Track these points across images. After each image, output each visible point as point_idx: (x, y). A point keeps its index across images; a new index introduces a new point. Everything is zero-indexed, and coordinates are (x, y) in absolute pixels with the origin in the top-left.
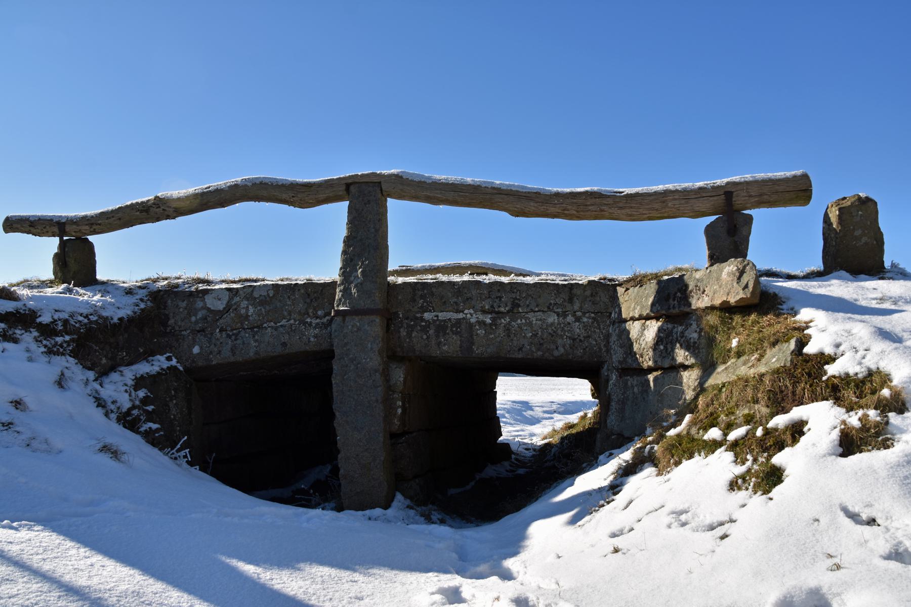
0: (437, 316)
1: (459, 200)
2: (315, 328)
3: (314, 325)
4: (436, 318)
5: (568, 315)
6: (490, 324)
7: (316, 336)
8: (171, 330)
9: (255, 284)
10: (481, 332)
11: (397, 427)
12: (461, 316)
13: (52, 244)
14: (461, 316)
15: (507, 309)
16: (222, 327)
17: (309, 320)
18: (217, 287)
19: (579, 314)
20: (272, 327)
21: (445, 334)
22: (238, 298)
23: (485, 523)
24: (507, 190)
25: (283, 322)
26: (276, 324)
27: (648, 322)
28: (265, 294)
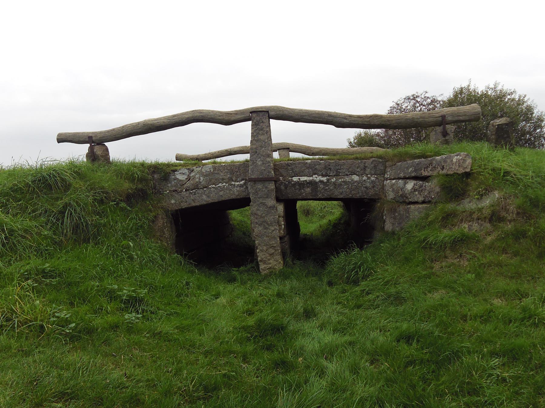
0: (299, 179)
1: (105, 201)
2: (237, 187)
3: (236, 186)
4: (299, 180)
5: (364, 177)
6: (326, 182)
7: (238, 191)
8: (158, 191)
9: (331, 161)
10: (322, 186)
11: (282, 234)
12: (311, 178)
13: (85, 148)
14: (311, 178)
15: (334, 174)
16: (187, 189)
17: (233, 183)
18: (236, 164)
19: (369, 175)
20: (214, 188)
21: (304, 187)
22: (194, 173)
23: (181, 156)
24: (238, 149)
25: (220, 185)
26: (216, 185)
27: (408, 181)
28: (209, 170)
